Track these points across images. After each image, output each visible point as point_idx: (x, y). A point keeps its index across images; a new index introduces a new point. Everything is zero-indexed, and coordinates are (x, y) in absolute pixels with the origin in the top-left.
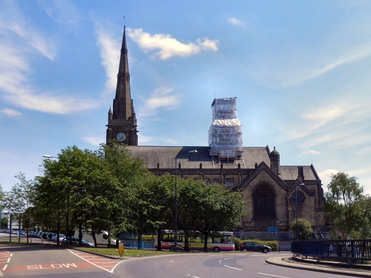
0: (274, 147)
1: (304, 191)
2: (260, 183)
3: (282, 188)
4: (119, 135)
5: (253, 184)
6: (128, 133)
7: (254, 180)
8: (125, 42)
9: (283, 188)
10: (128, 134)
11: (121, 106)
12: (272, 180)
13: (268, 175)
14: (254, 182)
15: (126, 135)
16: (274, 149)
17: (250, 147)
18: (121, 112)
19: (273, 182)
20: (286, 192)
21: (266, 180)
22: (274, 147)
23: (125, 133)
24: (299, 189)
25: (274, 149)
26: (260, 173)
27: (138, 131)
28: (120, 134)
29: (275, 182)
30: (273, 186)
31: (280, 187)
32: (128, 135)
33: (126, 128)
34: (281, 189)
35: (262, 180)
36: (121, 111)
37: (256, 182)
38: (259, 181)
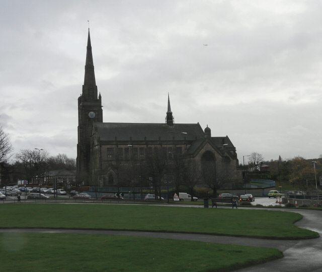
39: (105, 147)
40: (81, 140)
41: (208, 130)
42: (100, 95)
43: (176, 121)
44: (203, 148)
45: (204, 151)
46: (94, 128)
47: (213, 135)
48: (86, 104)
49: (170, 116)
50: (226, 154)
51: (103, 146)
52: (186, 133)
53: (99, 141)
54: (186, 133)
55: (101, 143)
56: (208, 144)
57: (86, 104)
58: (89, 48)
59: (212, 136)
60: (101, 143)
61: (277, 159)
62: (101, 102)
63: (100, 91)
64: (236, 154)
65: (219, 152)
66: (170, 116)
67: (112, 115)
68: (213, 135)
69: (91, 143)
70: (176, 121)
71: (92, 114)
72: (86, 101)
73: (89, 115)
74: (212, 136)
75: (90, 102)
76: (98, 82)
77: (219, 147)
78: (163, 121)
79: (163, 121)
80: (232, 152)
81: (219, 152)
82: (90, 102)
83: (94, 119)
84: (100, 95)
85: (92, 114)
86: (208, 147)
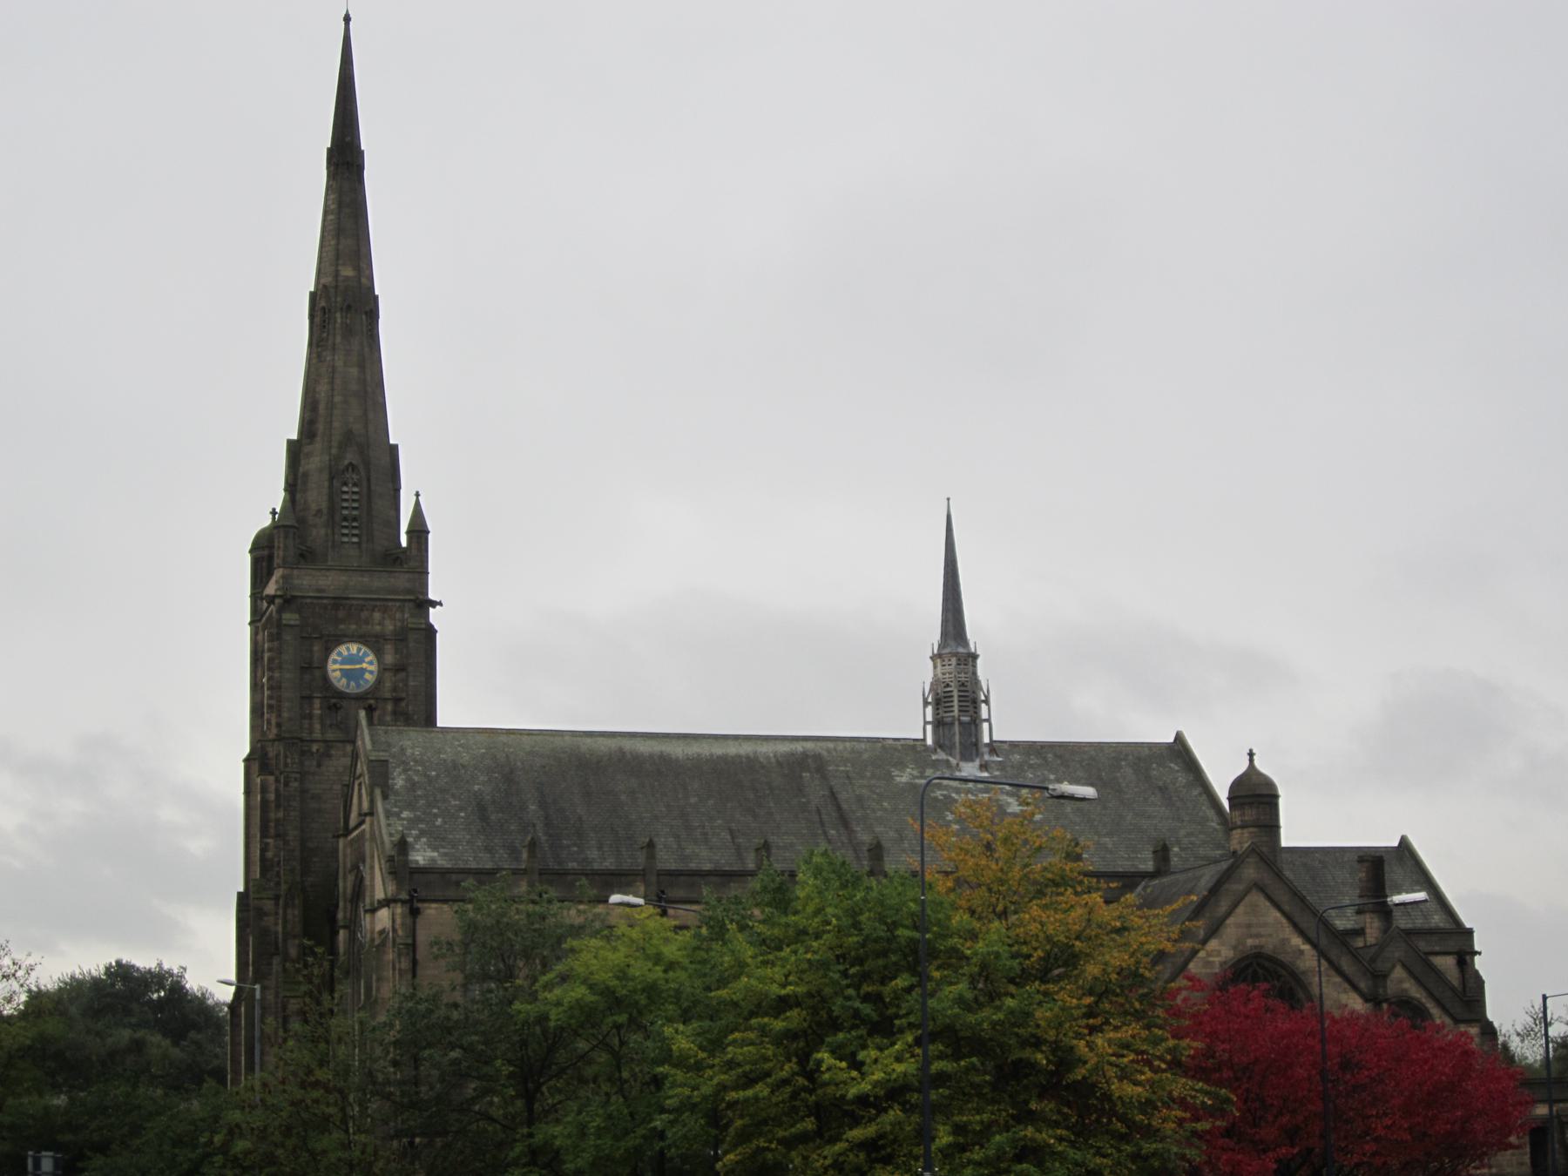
0: (1251, 754)
1: (1431, 995)
2: (1239, 961)
3: (1346, 986)
4: (366, 655)
5: (1208, 964)
6: (389, 648)
7: (1213, 944)
8: (604, 745)
9: (1355, 988)
10: (389, 648)
11: (345, 484)
12: (1297, 941)
13: (1278, 915)
14: (1209, 954)
15: (379, 653)
16: (1251, 760)
17: (736, 738)
18: (345, 519)
19: (1302, 952)
20: (1369, 1005)
21: (1269, 945)
22: (1251, 754)
23: (374, 642)
24: (1406, 985)
25: (1251, 760)
26: (1240, 909)
27: (440, 604)
28: (371, 663)
29: (1314, 952)
30: (1304, 973)
31: (1338, 979)
32: (389, 659)
33: (377, 615)
34: (1345, 992)
35: (1250, 942)
36: (345, 512)
37: (1219, 953)
38: (1235, 948)
39: (439, 919)
40: (266, 866)
41: (1256, 796)
42: (418, 513)
43: (1009, 719)
44: (1214, 931)
45: (1227, 953)
46: (361, 767)
47: (1296, 831)
48: (310, 581)
49: (957, 697)
50: (1400, 981)
51: (431, 911)
52: (1088, 791)
53: (399, 867)
54: (1088, 791)
55: (416, 890)
56: (1257, 898)
57: (310, 581)
58: (345, 159)
59: (1284, 843)
60: (416, 890)
61: (1477, 948)
62: (422, 572)
63: (421, 482)
64: (1480, 983)
65: (1346, 964)
66: (957, 697)
67: (509, 660)
68: (1296, 831)
69: (345, 885)
70: (1009, 719)
71: (352, 664)
72: (306, 556)
73: (335, 668)
74: (1284, 843)
75: (339, 565)
76: (405, 422)
77: (1341, 924)
78: (906, 719)
79: (906, 719)
80: (1446, 963)
81: (1346, 964)
82: (339, 565)
83: (370, 701)
84: (418, 513)
85: (352, 664)
86: (1259, 925)
